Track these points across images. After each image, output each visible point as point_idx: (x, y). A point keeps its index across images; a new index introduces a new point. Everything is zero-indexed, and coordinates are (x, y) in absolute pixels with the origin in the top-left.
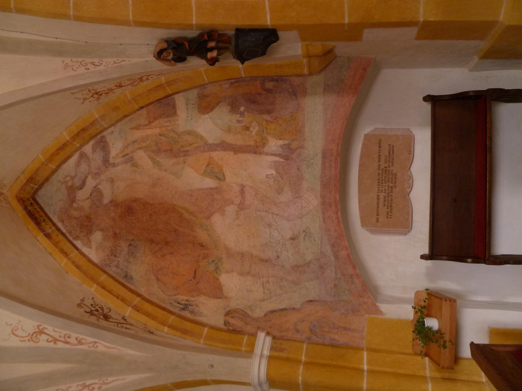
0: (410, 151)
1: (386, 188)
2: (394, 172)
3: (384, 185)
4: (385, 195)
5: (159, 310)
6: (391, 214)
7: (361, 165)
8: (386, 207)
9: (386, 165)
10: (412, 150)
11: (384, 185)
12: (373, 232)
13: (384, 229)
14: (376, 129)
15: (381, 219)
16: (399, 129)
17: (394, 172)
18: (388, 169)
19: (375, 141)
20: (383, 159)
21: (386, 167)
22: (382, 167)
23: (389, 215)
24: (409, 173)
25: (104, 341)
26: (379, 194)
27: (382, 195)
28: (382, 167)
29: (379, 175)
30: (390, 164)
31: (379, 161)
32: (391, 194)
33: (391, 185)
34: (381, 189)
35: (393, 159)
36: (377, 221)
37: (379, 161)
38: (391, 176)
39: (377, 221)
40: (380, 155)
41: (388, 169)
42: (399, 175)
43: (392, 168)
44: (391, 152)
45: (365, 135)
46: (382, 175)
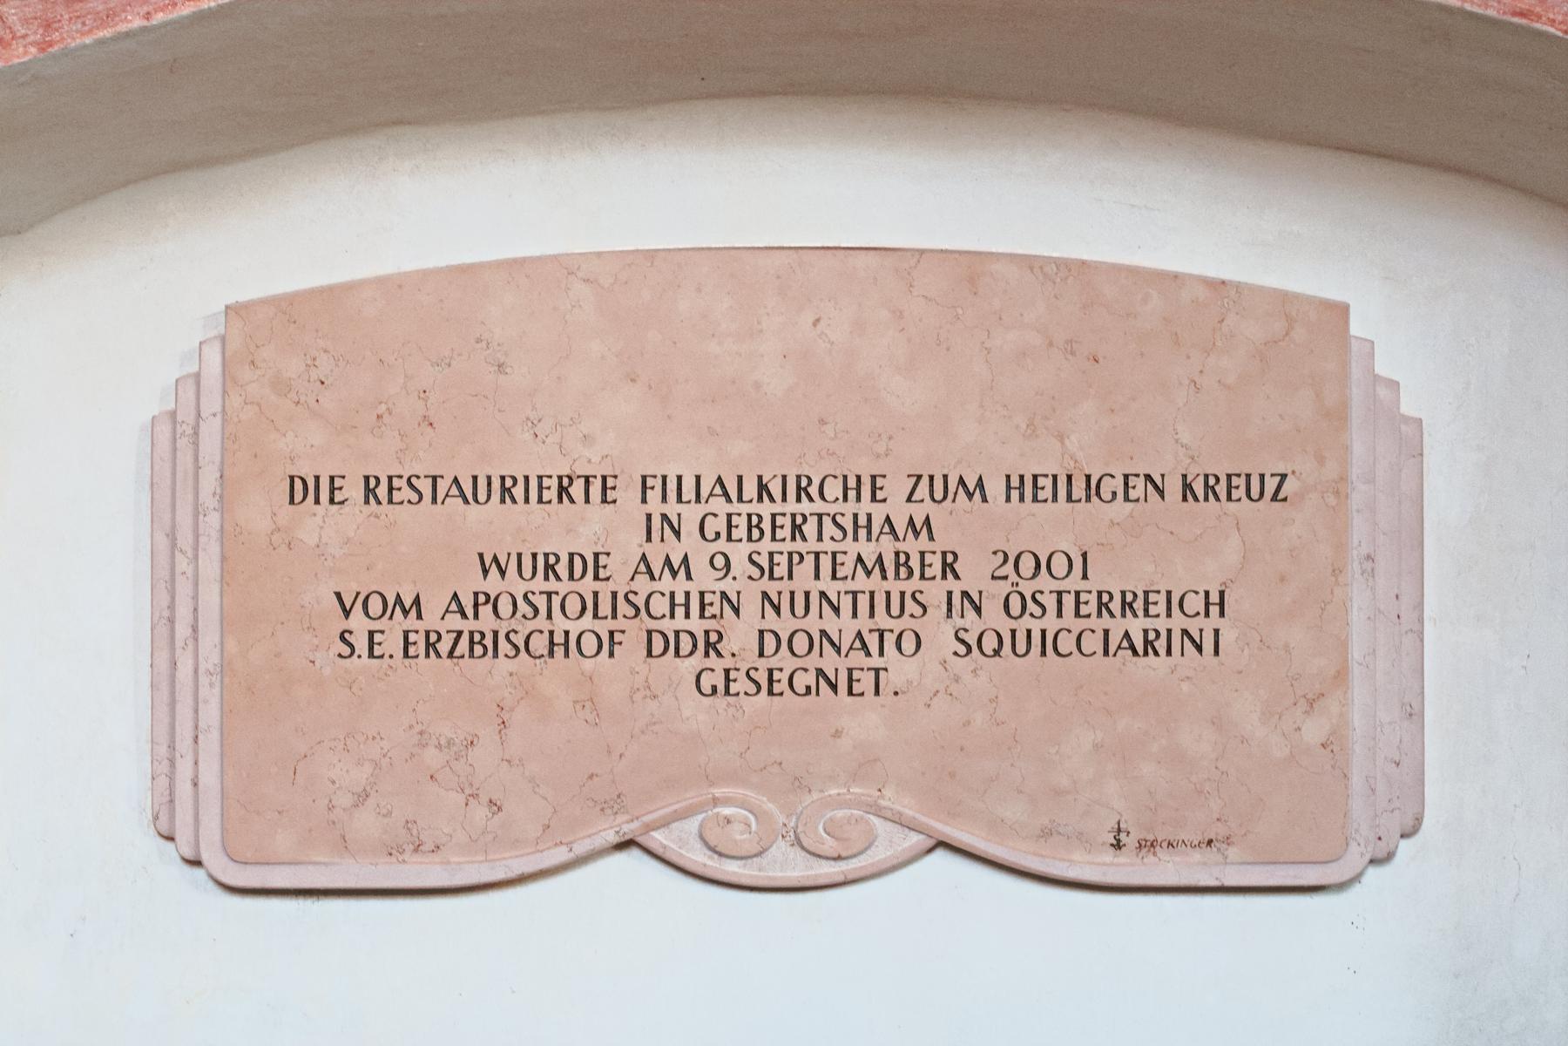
0: (1148, 846)
1: (705, 578)
2: (899, 669)
3: (739, 553)
4: (619, 569)
5: (191, 812)
6: (391, 643)
7: (971, 268)
8: (470, 583)
9: (974, 575)
10: (1165, 870)
11: (739, 553)
12: (175, 433)
13: (210, 566)
14: (1409, 442)
15: (315, 522)
16: (1414, 715)
17: (899, 669)
18: (934, 593)
19: (1277, 448)
20: (1050, 527)
21: (949, 568)
22: (956, 526)
23: (378, 619)
24: (890, 842)
25: (226, 712)
26: (627, 494)
27: (612, 531)
28: (956, 526)
29: (851, 488)
30: (994, 616)
31: (1022, 487)
32: (633, 634)
33: (740, 635)
34: (690, 515)
35: (1048, 644)
36: (301, 489)
37: (1022, 487)
38: (844, 626)
39: (301, 489)
40: (1093, 489)
41: (934, 593)
42: (862, 720)
43: (939, 632)
44: (1136, 626)
45: (1341, 311)
46: (862, 527)
